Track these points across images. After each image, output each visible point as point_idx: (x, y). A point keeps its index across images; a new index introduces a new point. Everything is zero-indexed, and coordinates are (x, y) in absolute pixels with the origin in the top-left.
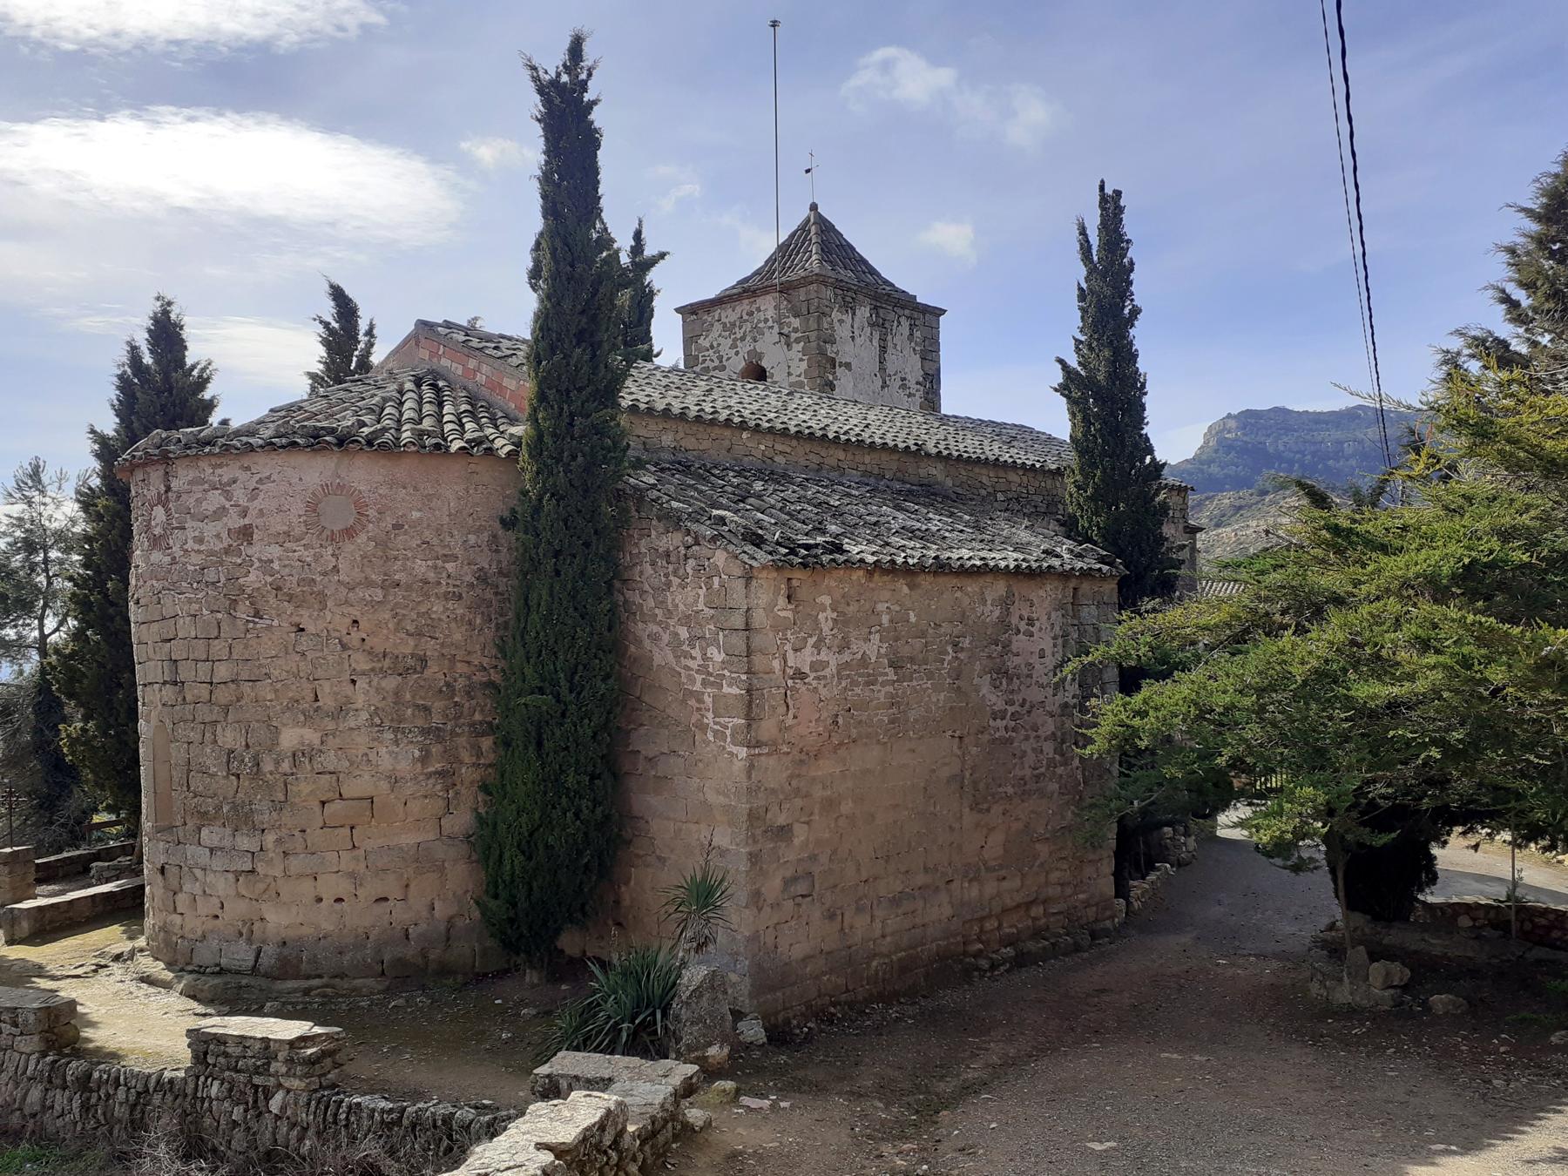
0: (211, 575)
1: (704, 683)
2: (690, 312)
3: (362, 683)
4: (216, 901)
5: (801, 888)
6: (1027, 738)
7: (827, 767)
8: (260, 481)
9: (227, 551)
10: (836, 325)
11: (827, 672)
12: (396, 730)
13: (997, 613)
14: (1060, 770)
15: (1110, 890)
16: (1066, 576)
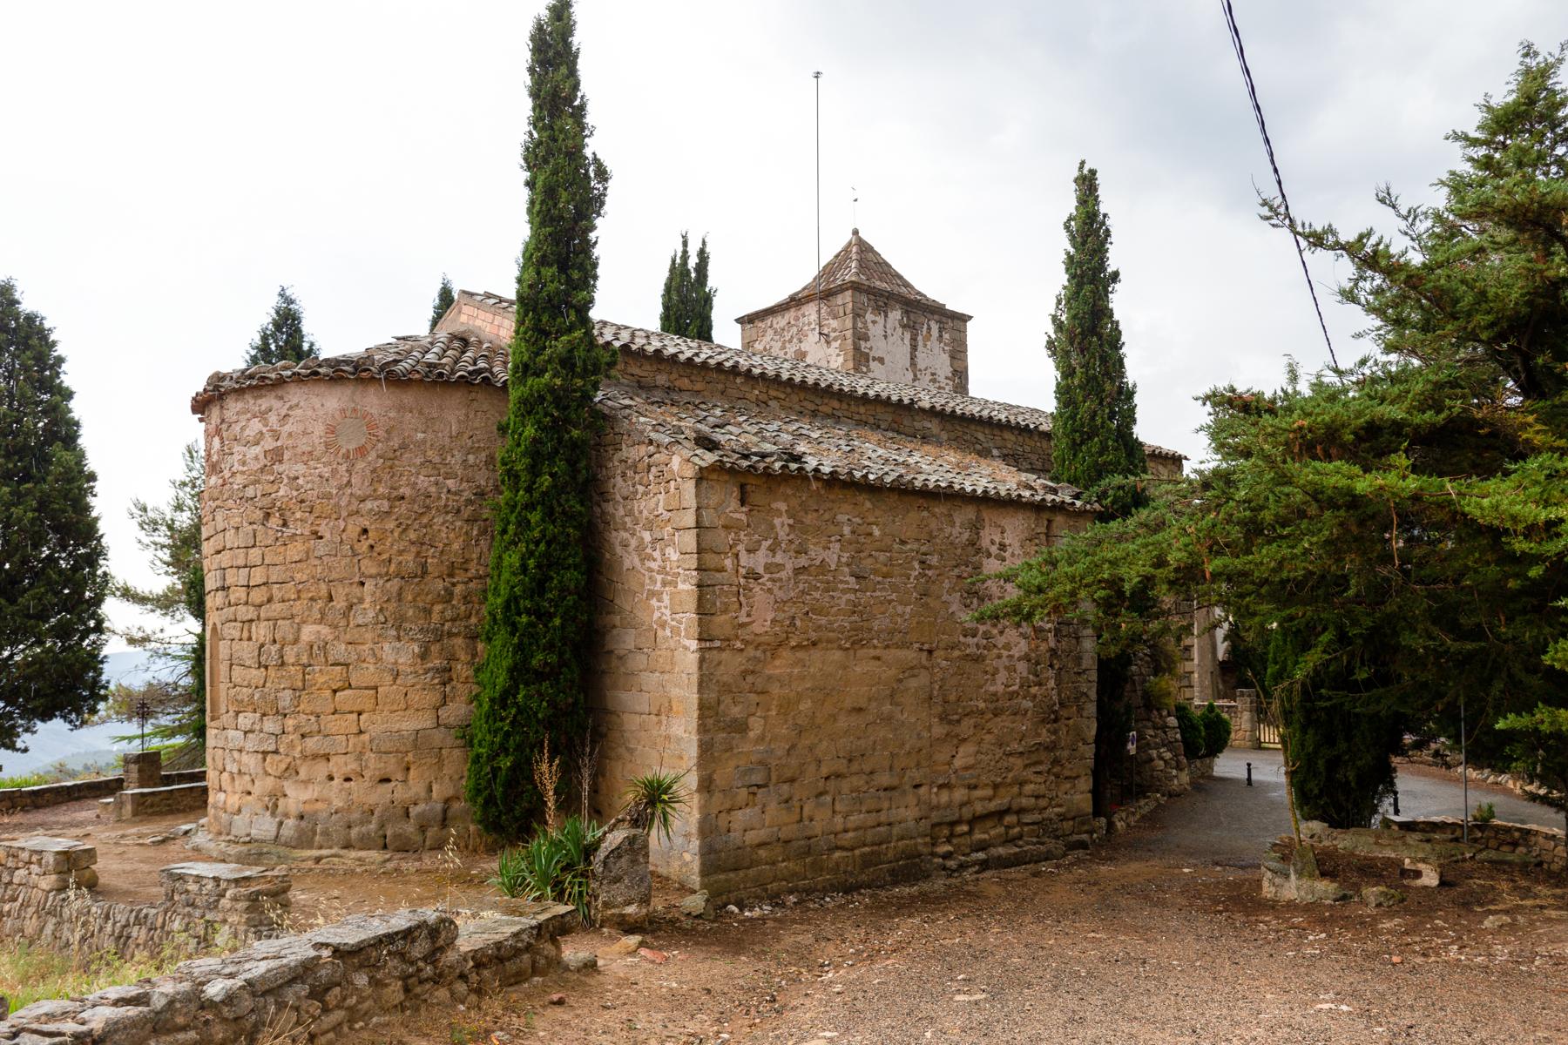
0: (250, 492)
1: (664, 584)
2: (747, 321)
3: (369, 585)
4: (247, 778)
5: (757, 778)
6: (999, 657)
7: (780, 666)
8: (291, 408)
9: (262, 470)
10: (870, 325)
11: (783, 575)
12: (399, 628)
13: (966, 535)
14: (1034, 690)
15: (1087, 806)
16: (1038, 508)
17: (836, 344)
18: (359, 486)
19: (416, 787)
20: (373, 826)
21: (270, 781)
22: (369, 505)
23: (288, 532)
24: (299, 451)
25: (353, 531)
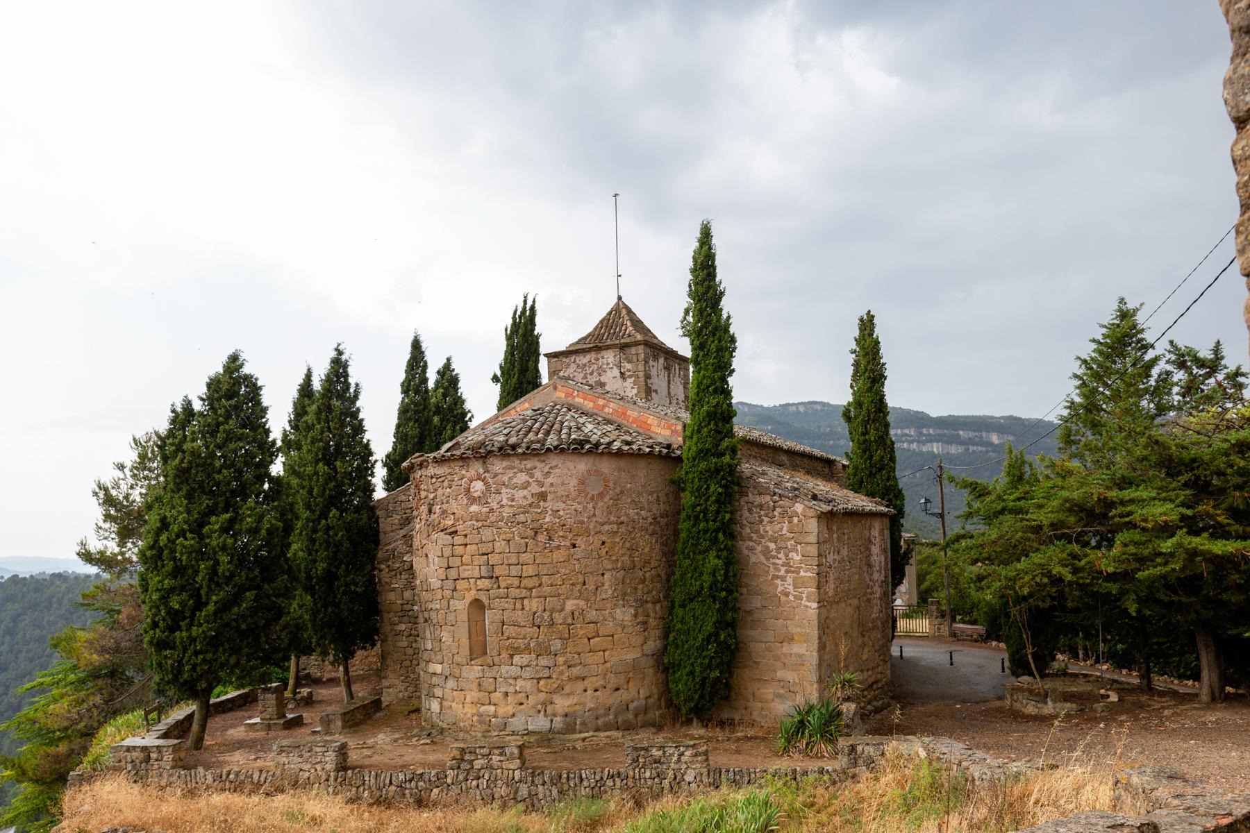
0: (521, 518)
1: (787, 572)
17: (629, 380)
18: (600, 516)
19: (633, 693)
20: (611, 717)
21: (542, 696)
22: (606, 527)
23: (554, 544)
24: (559, 494)
25: (598, 543)
